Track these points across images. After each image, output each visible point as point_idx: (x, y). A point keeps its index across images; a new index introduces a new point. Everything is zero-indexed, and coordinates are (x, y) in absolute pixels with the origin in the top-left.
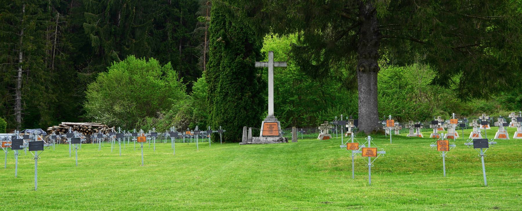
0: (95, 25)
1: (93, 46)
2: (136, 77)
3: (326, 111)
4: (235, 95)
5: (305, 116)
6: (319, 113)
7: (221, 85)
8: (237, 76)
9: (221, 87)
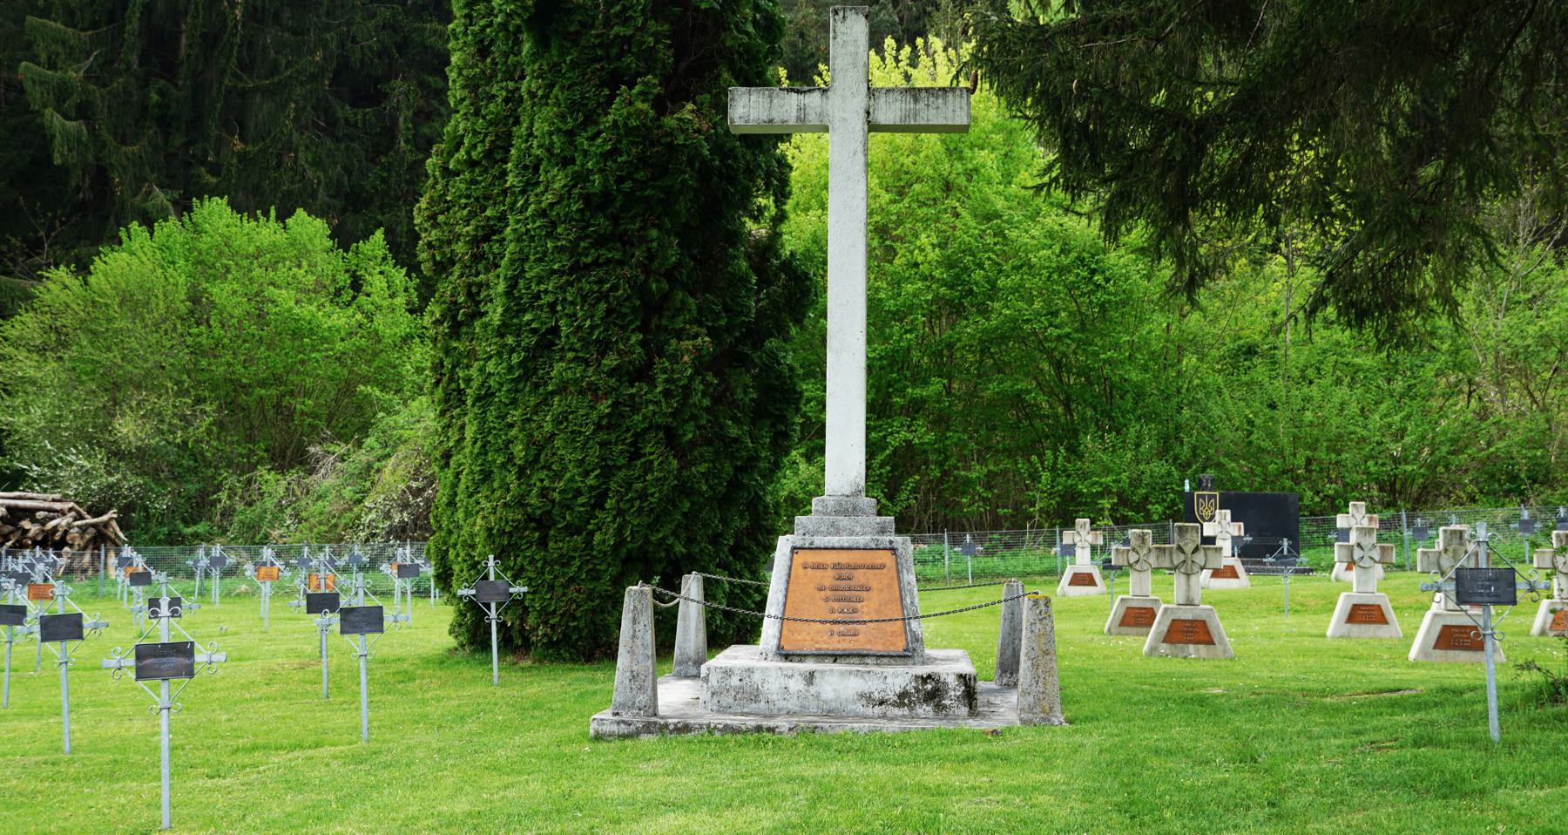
0: (74, 74)
1: (57, 161)
2: (220, 292)
3: (1073, 450)
4: (604, 347)
5: (977, 472)
6: (1041, 456)
7: (512, 285)
8: (615, 219)
9: (509, 293)
